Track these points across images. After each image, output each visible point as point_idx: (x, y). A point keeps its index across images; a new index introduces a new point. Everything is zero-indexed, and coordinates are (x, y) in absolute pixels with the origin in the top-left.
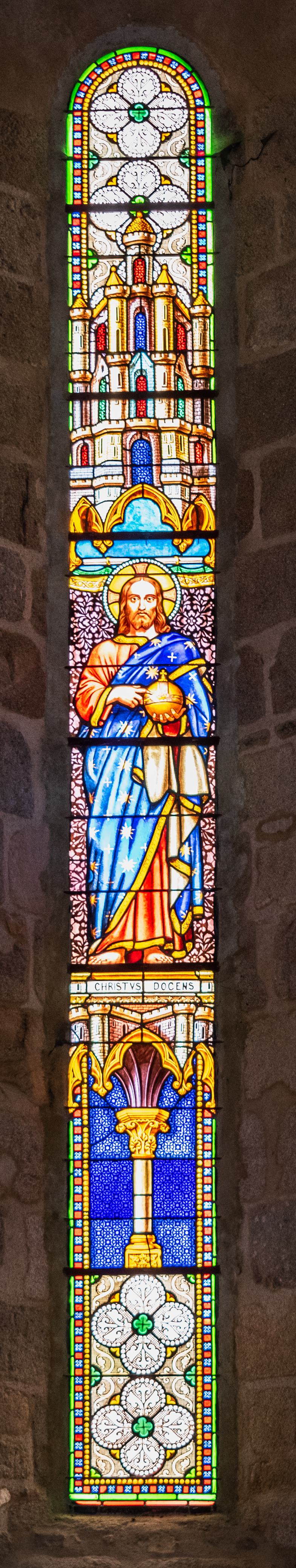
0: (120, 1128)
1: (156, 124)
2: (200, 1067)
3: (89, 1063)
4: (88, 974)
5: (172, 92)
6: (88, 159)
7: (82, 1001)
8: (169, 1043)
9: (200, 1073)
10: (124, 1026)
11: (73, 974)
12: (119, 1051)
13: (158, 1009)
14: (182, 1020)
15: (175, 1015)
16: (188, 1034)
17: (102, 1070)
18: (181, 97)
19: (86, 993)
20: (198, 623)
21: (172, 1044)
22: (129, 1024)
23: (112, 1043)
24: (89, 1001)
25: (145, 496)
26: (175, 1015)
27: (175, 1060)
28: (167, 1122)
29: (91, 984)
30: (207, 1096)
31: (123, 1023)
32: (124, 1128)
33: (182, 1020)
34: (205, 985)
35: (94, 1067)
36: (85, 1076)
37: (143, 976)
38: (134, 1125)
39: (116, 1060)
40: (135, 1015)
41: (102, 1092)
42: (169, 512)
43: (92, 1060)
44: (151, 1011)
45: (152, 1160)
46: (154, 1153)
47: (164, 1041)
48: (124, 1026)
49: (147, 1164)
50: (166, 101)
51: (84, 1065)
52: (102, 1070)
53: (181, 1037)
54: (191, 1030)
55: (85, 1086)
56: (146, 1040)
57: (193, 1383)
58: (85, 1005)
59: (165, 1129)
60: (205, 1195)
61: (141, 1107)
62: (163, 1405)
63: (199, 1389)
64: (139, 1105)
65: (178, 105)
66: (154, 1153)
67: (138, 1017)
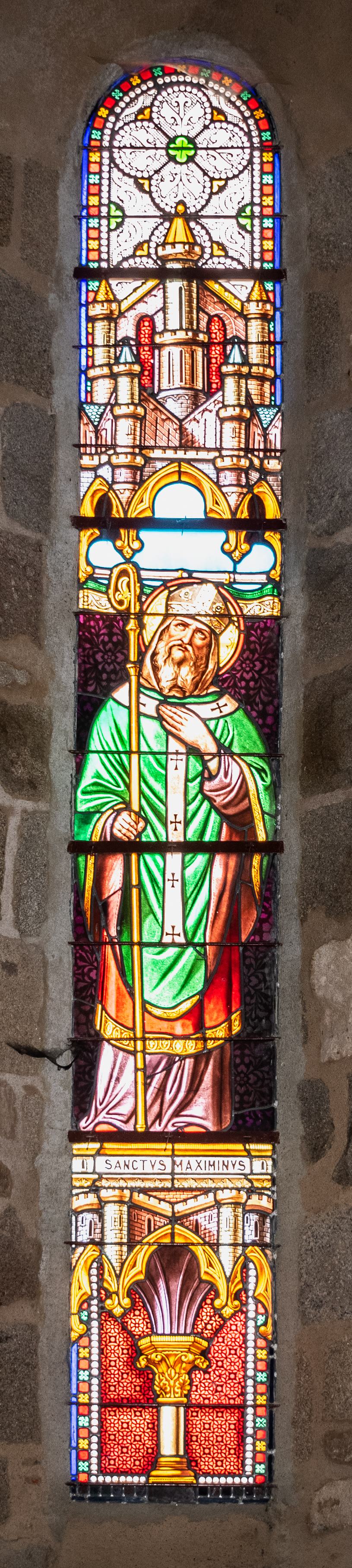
0: (142, 1362)
2: (252, 1280)
3: (101, 1268)
4: (97, 1145)
8: (211, 1245)
10: (149, 1220)
11: (76, 1146)
12: (142, 1254)
14: (227, 1212)
15: (218, 1204)
16: (235, 1231)
18: (241, 129)
19: (94, 1172)
20: (251, 1081)
23: (131, 1244)
24: (97, 1184)
25: (183, 478)
26: (218, 1204)
27: (217, 1268)
29: (100, 1160)
30: (261, 1319)
31: (148, 1216)
33: (227, 1212)
34: (257, 1165)
35: (106, 1276)
36: (95, 1286)
37: (173, 1150)
43: (98, 1264)
47: (205, 1243)
50: (219, 135)
51: (94, 1272)
52: (118, 1277)
53: (226, 1237)
54: (240, 1226)
55: (95, 1302)
56: (178, 1240)
57: (249, 228)
58: (94, 1189)
60: (97, 170)
61: (171, 1334)
63: (257, 235)
64: (167, 1331)
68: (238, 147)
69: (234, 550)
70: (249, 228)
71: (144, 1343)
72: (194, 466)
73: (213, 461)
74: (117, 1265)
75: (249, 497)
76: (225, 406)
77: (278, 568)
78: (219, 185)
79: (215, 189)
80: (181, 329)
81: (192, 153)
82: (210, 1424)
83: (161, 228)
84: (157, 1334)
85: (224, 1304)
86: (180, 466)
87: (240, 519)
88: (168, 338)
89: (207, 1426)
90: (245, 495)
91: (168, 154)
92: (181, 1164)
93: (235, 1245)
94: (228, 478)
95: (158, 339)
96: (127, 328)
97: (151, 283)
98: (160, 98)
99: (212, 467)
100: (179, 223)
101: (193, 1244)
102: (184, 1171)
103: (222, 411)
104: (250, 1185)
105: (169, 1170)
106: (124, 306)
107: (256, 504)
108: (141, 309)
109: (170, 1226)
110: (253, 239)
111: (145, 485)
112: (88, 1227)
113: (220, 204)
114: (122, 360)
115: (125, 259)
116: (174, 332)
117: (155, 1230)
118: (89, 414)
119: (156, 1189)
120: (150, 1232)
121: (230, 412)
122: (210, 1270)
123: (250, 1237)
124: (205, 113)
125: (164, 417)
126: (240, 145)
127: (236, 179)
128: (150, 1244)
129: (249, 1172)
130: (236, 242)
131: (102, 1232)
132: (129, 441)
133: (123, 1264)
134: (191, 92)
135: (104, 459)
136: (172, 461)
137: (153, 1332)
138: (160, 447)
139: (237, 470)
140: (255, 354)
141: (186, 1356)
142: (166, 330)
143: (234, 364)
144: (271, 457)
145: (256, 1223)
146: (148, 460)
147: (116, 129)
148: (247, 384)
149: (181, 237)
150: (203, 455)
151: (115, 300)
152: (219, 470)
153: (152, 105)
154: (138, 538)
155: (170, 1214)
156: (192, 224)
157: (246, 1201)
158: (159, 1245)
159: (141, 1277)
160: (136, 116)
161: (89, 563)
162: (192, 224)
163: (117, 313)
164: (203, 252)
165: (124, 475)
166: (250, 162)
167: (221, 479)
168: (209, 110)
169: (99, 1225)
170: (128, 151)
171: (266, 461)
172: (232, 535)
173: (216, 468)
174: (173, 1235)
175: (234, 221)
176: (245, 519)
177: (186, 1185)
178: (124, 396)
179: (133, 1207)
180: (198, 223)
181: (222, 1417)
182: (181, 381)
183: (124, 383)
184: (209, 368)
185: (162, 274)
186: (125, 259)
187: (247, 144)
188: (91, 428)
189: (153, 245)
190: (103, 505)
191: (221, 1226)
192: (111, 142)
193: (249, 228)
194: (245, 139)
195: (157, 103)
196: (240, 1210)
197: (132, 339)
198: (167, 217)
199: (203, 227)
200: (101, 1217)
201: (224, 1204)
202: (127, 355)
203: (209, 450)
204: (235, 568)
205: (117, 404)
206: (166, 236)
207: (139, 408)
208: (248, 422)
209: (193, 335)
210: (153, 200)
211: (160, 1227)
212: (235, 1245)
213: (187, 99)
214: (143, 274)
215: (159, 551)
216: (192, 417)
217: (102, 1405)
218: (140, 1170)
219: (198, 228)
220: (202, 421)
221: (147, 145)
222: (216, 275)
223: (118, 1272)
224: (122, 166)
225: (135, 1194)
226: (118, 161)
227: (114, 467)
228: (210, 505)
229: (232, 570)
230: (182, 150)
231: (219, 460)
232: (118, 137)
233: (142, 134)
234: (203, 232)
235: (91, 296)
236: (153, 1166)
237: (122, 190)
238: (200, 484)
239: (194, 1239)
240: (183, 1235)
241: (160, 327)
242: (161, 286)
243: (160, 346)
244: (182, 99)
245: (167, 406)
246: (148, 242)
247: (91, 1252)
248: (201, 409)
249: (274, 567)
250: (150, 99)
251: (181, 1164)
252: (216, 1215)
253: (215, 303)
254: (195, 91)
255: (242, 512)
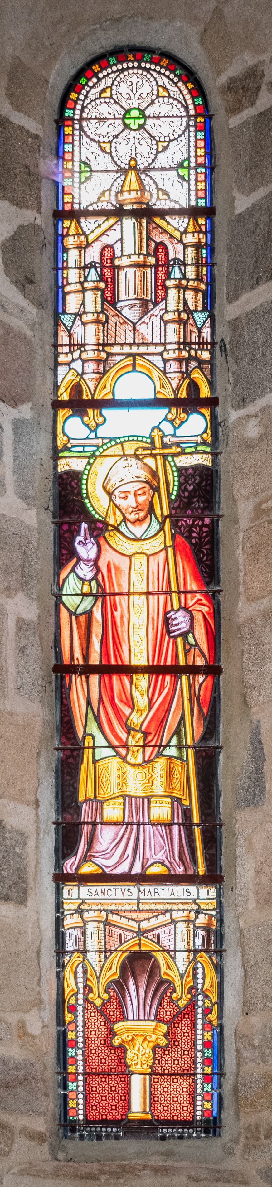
0: (116, 1042)
1: (154, 133)
2: (200, 976)
5: (169, 97)
6: (80, 172)
7: (75, 907)
9: (200, 981)
10: (120, 934)
12: (116, 961)
13: (156, 916)
15: (173, 922)
17: (98, 978)
18: (179, 102)
21: (172, 954)
22: (127, 933)
24: (82, 907)
28: (166, 1035)
31: (121, 932)
32: (120, 1040)
38: (130, 1038)
39: (113, 972)
40: (131, 923)
41: (98, 1002)
42: (169, 967)
44: (148, 919)
45: (150, 1075)
46: (151, 1067)
47: (164, 950)
48: (120, 934)
49: (145, 1079)
50: (162, 107)
51: (80, 975)
53: (182, 946)
57: (186, 178)
59: (163, 1042)
62: (154, 97)
63: (193, 182)
64: (136, 1018)
65: (176, 112)
66: (151, 1067)
67: (135, 925)
68: (177, 116)
69: (175, 419)
70: (187, 178)
71: (117, 1027)
72: (145, 358)
73: (161, 354)
74: (97, 969)
75: (187, 382)
76: (167, 311)
77: (209, 431)
78: (162, 146)
79: (160, 149)
80: (135, 254)
81: (142, 121)
82: (168, 1088)
83: (119, 180)
84: (128, 1020)
85: (179, 997)
86: (134, 360)
87: (181, 398)
88: (125, 261)
89: (166, 1090)
90: (184, 379)
91: (124, 124)
92: (144, 890)
93: (188, 951)
94: (173, 366)
95: (117, 262)
96: (93, 254)
97: (112, 221)
98: (118, 79)
99: (160, 358)
100: (132, 175)
101: (154, 951)
102: (146, 897)
103: (166, 315)
104: (197, 907)
105: (135, 896)
106: (91, 238)
107: (194, 387)
108: (105, 240)
109: (137, 938)
110: (189, 185)
111: (108, 374)
112: (73, 941)
113: (163, 160)
114: (89, 279)
115: (91, 205)
116: (129, 256)
117: (125, 942)
118: (64, 322)
119: (125, 911)
120: (121, 944)
121: (171, 316)
122: (168, 971)
123: (199, 945)
124: (152, 90)
125: (121, 321)
126: (179, 114)
127: (176, 141)
128: (124, 952)
129: (196, 897)
130: (177, 191)
131: (85, 944)
132: (94, 341)
133: (101, 969)
134: (142, 74)
135: (76, 355)
136: (128, 355)
137: (124, 1018)
138: (119, 344)
139: (179, 360)
140: (191, 272)
141: (150, 1036)
142: (122, 255)
143: (175, 279)
144: (203, 349)
145: (203, 936)
146: (109, 354)
147: (85, 105)
148: (184, 294)
149: (135, 186)
150: (152, 349)
151: (84, 234)
152: (165, 361)
153: (113, 84)
154: (101, 415)
155: (136, 930)
156: (143, 176)
157: (195, 920)
158: (130, 952)
159: (116, 977)
160: (100, 94)
161: (64, 434)
162: (143, 176)
163: (85, 243)
164: (151, 195)
165: (91, 367)
166: (188, 126)
167: (167, 368)
168: (155, 88)
169: (82, 939)
170: (94, 122)
171: (199, 352)
172: (174, 410)
173: (163, 359)
174: (139, 944)
175: (175, 173)
176: (184, 398)
177: (147, 907)
178: (90, 307)
179: (107, 923)
180: (147, 175)
181: (177, 1082)
182: (135, 293)
183: (89, 296)
184: (156, 282)
185: (119, 213)
186: (91, 205)
187: (184, 114)
188: (67, 334)
189: (113, 194)
190: (77, 389)
191: (177, 938)
192: (81, 115)
193: (187, 178)
194: (182, 110)
195: (116, 83)
196: (192, 926)
197: (98, 263)
198: (125, 172)
199: (151, 178)
200: (84, 933)
201: (179, 921)
202: (93, 275)
203: (156, 344)
204: (175, 432)
205: (85, 313)
206: (122, 186)
207: (101, 315)
208: (185, 323)
209: (145, 258)
210: (112, 158)
211: (129, 940)
212: (188, 951)
213: (139, 80)
214: (105, 213)
215: (116, 423)
216: (143, 320)
217: (85, 1074)
218: (113, 897)
219: (148, 179)
220: (150, 324)
221: (108, 116)
222: (162, 213)
223: (98, 974)
224: (89, 133)
225: (110, 915)
226: (86, 129)
227: (84, 361)
228: (158, 389)
229: (173, 433)
230: (135, 119)
231: (165, 353)
232: (86, 110)
233: (104, 110)
234: (151, 182)
235: (65, 231)
236: (123, 893)
237: (89, 150)
238: (150, 372)
239: (156, 947)
240: (147, 945)
241: (118, 253)
242: (119, 223)
243: (119, 268)
244: (134, 79)
245: (123, 312)
246: (110, 190)
247: (77, 958)
248: (149, 314)
249: (205, 432)
250: (111, 81)
251: (144, 890)
252: (173, 929)
253: (160, 233)
254: (145, 73)
255: (181, 394)
